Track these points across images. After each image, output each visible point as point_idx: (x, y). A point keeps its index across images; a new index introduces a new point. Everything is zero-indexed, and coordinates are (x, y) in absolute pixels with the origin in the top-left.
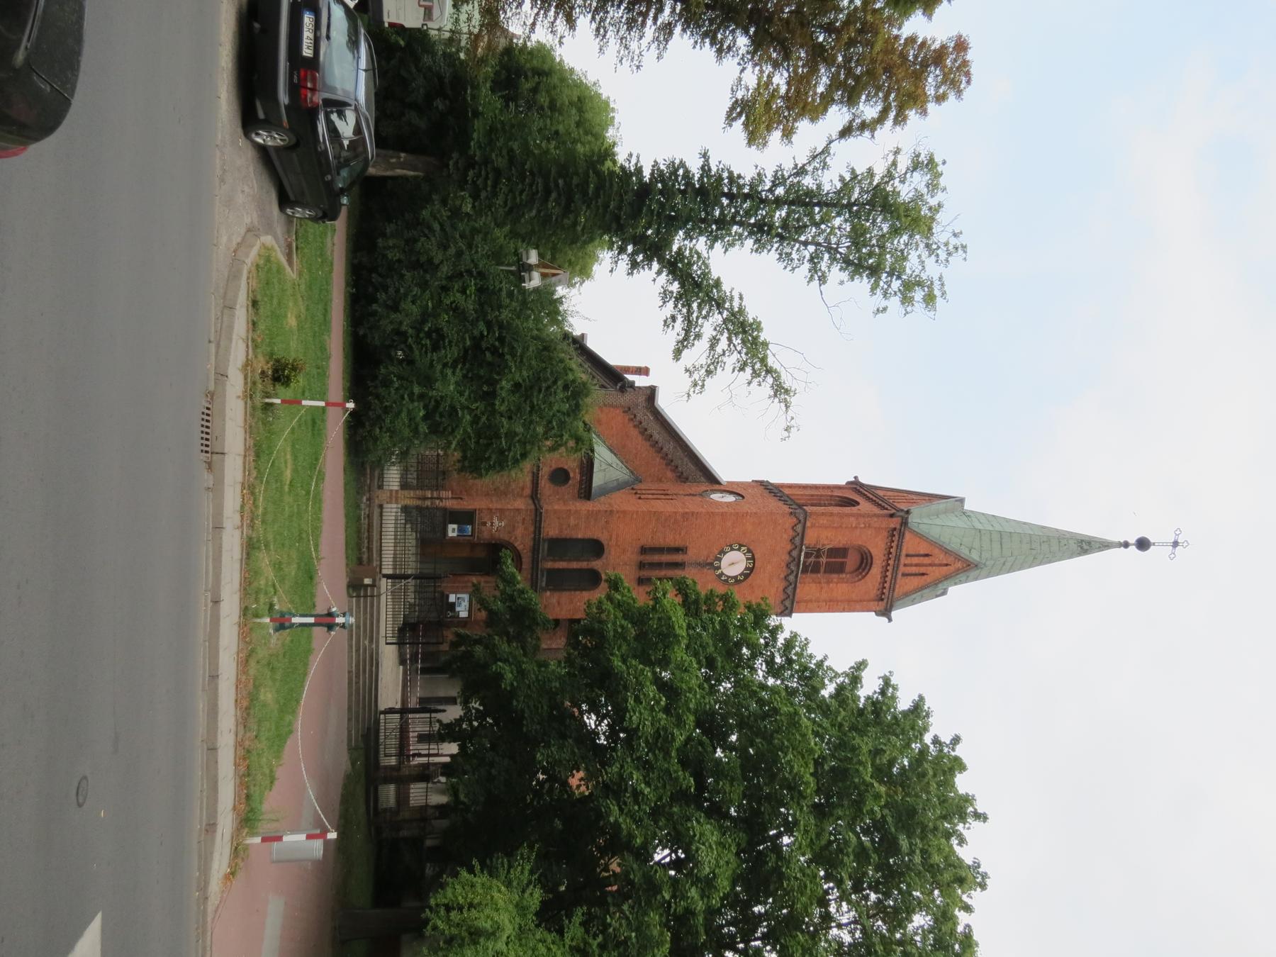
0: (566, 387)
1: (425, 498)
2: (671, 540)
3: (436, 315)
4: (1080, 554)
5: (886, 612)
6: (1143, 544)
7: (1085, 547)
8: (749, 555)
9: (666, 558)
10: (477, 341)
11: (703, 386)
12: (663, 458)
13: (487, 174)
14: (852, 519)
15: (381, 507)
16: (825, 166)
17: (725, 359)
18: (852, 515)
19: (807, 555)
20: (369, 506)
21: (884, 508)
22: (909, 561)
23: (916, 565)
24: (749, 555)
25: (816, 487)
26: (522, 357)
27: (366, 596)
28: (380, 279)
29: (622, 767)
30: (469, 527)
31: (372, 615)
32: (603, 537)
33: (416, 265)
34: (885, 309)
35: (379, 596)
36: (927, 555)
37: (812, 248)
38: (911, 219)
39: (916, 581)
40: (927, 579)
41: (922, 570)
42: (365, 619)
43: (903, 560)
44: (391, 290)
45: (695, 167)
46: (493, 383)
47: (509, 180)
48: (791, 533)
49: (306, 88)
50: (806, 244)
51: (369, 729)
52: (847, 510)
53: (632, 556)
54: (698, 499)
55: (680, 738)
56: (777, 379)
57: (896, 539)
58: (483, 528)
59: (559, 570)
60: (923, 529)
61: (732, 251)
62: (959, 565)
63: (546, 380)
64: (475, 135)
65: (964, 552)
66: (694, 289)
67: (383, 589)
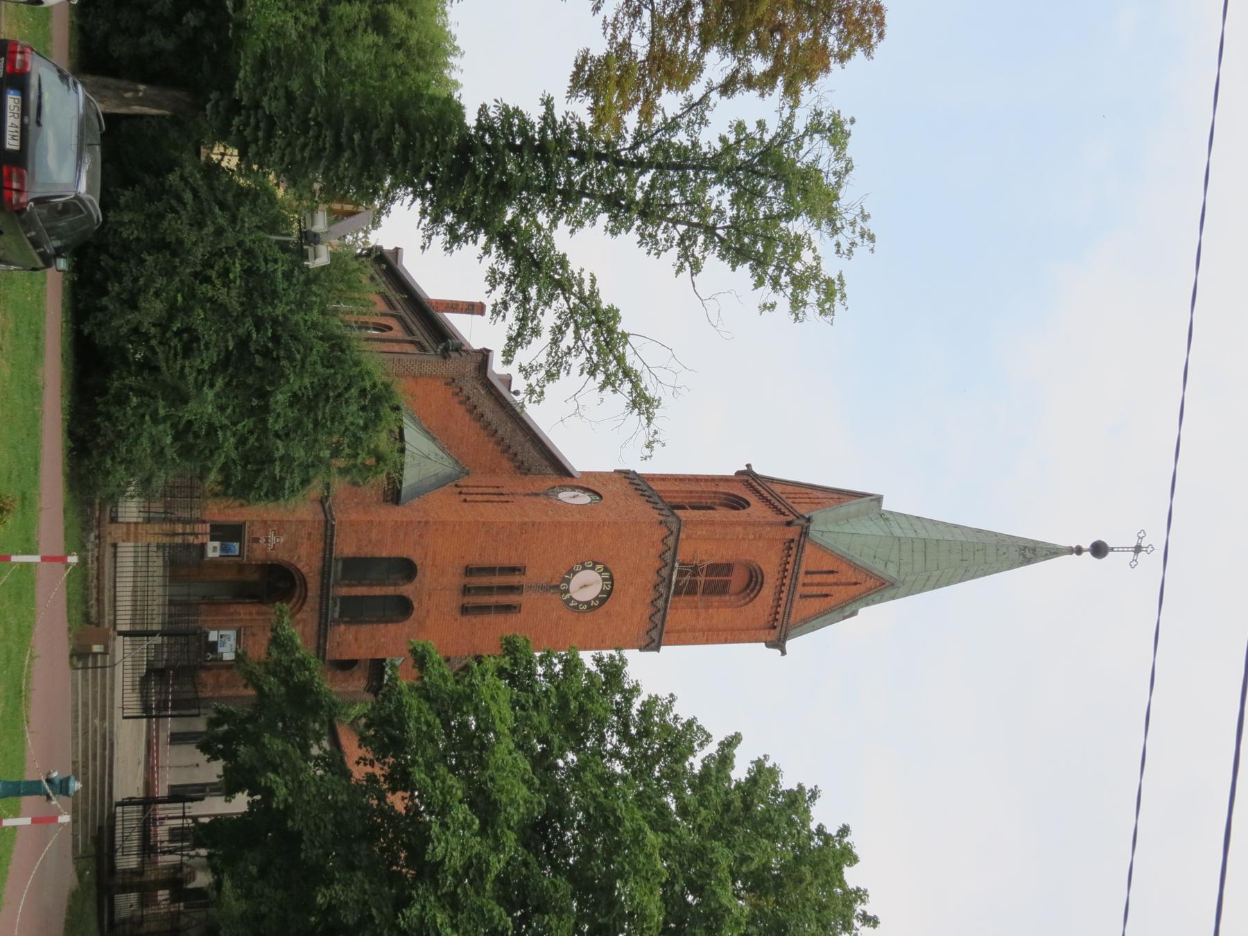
0: (363, 392)
1: (175, 534)
2: (504, 557)
3: (187, 310)
4: (1021, 564)
5: (778, 644)
6: (1099, 550)
7: (1029, 555)
8: (606, 575)
9: (497, 580)
10: (243, 343)
11: (542, 393)
12: (498, 443)
13: (258, 122)
14: (739, 529)
15: (115, 546)
16: (703, 121)
17: (571, 360)
18: (739, 523)
19: (681, 574)
20: (98, 546)
21: (783, 514)
22: (808, 579)
23: (818, 584)
24: (606, 575)
25: (696, 479)
26: (303, 361)
27: (95, 667)
28: (111, 262)
29: (424, 907)
30: (236, 545)
31: (104, 687)
32: (416, 557)
33: (161, 245)
34: (773, 306)
35: (113, 666)
36: (832, 572)
37: (682, 228)
38: (813, 194)
39: (817, 604)
40: (830, 601)
41: (825, 590)
42: (95, 693)
43: (802, 578)
44: (127, 281)
45: (535, 114)
46: (263, 395)
47: (286, 131)
48: (661, 547)
49: (11, 189)
50: (675, 221)
51: (101, 828)
52: (733, 515)
53: (454, 579)
54: (543, 500)
55: (497, 864)
56: (635, 386)
57: (793, 552)
58: (255, 545)
59: (356, 597)
60: (827, 541)
61: (580, 232)
62: (870, 583)
63: (336, 387)
64: (241, 74)
65: (878, 568)
66: (533, 270)
67: (119, 656)
